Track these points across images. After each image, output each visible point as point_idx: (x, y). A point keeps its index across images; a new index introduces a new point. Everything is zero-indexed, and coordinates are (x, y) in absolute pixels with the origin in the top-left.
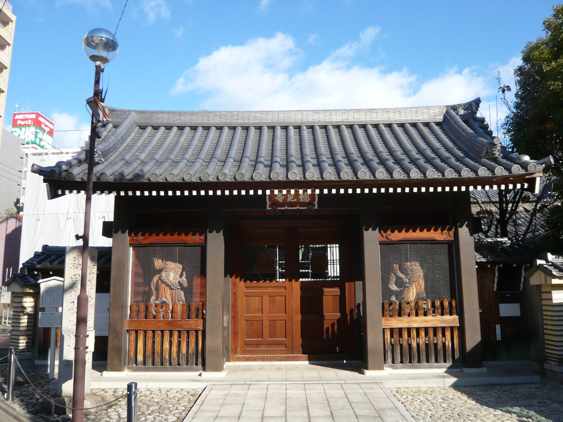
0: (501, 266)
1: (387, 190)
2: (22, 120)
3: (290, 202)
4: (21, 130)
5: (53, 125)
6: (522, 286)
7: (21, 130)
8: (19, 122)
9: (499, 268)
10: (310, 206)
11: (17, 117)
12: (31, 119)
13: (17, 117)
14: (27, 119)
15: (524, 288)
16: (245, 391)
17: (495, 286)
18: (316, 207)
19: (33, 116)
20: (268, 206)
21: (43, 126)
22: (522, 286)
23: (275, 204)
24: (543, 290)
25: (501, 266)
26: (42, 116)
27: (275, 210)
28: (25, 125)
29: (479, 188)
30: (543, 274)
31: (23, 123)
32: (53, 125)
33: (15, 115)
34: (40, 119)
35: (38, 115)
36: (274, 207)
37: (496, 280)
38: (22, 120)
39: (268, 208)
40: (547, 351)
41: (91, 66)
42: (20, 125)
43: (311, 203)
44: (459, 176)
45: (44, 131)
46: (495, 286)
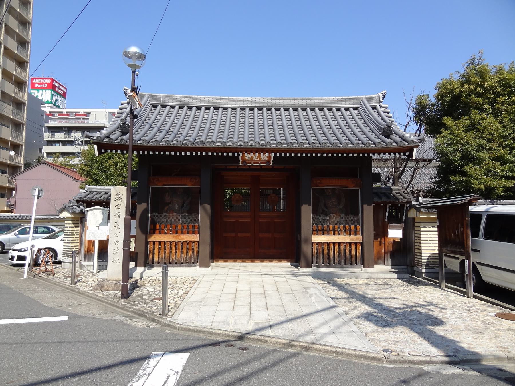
0: (390, 205)
1: (170, 153)
2: (39, 84)
3: (255, 160)
4: (38, 92)
5: (66, 89)
6: (404, 218)
7: (38, 92)
8: (36, 85)
9: (389, 206)
10: (268, 163)
11: (34, 81)
12: (47, 83)
13: (34, 81)
14: (43, 83)
15: (405, 220)
16: (225, 278)
17: (386, 218)
18: (272, 164)
19: (49, 81)
20: (240, 163)
21: (57, 89)
22: (404, 218)
23: (245, 161)
24: (415, 221)
25: (390, 205)
26: (56, 82)
27: (245, 165)
28: (42, 88)
29: (119, 152)
30: (415, 211)
31: (40, 86)
32: (66, 89)
33: (33, 79)
34: (54, 83)
35: (53, 80)
36: (245, 163)
37: (387, 214)
38: (39, 84)
39: (240, 164)
40: (416, 259)
41: (130, 70)
42: (37, 88)
43: (268, 162)
44: (78, 156)
45: (59, 94)
46: (386, 218)
